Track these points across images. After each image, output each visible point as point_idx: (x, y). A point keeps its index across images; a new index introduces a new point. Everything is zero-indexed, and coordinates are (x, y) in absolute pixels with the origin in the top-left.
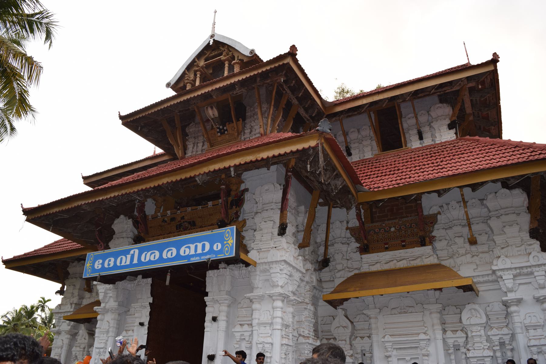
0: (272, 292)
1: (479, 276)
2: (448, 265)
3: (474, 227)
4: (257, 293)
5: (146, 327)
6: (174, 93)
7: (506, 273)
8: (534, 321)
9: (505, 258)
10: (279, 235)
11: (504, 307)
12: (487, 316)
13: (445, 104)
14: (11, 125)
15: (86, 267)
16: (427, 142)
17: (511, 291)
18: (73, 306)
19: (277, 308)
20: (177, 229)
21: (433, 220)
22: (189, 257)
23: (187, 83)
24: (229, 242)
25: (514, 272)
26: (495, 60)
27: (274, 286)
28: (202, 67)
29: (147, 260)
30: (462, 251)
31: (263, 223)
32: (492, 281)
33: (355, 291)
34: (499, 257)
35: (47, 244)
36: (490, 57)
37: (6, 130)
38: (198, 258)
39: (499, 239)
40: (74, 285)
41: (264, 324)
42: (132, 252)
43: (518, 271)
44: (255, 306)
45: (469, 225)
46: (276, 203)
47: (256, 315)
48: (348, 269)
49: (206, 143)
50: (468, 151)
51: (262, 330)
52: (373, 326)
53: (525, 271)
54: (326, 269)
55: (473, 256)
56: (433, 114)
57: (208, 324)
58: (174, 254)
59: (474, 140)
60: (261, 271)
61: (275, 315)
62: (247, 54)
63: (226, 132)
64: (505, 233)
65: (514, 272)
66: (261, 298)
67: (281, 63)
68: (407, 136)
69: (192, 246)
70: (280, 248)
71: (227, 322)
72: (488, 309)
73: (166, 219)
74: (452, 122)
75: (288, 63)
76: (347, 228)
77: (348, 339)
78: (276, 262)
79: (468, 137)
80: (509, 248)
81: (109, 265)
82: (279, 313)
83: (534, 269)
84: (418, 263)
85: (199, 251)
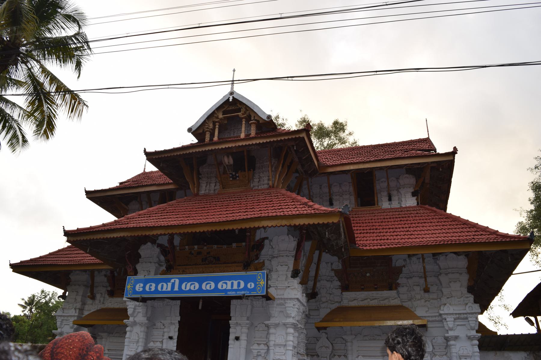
0: (287, 321)
1: (429, 316)
2: (407, 306)
3: (428, 279)
4: (273, 321)
5: (176, 341)
6: (195, 141)
7: (449, 317)
8: (465, 353)
9: (449, 306)
10: (292, 277)
11: (445, 341)
12: (433, 346)
13: (411, 176)
14: (23, 137)
15: (127, 288)
16: (395, 204)
17: (451, 329)
18: (77, 311)
19: (290, 334)
20: (202, 262)
21: (399, 271)
22: (226, 291)
23: (207, 131)
24: (261, 283)
25: (455, 316)
26: (455, 151)
27: (288, 316)
28: (221, 119)
29: (188, 289)
30: (418, 297)
31: (279, 266)
32: (438, 321)
33: (339, 321)
34: (445, 304)
35: (51, 251)
36: (451, 150)
37: (18, 142)
38: (234, 293)
39: (446, 291)
40: (77, 292)
41: (280, 345)
42: (172, 281)
43: (457, 316)
44: (272, 331)
45: (425, 278)
46: (289, 251)
47: (272, 338)
48: (329, 302)
49: (218, 184)
50: (426, 215)
51: (277, 349)
52: (349, 348)
53: (462, 316)
54: (314, 300)
55: (426, 301)
56: (402, 182)
57: (231, 342)
58: (213, 287)
59: (432, 210)
60: (277, 305)
61: (288, 339)
62: (265, 118)
63: (238, 178)
64: (450, 287)
65: (455, 316)
66: (277, 325)
67: (297, 136)
68: (379, 196)
69: (229, 283)
70: (293, 287)
71: (247, 341)
72: (433, 341)
73: (193, 252)
74: (415, 191)
75: (303, 138)
76: (332, 270)
77: (328, 357)
78: (291, 299)
79: (427, 206)
80: (453, 298)
81: (150, 289)
82: (291, 338)
83: (469, 315)
84: (386, 303)
85: (235, 287)
